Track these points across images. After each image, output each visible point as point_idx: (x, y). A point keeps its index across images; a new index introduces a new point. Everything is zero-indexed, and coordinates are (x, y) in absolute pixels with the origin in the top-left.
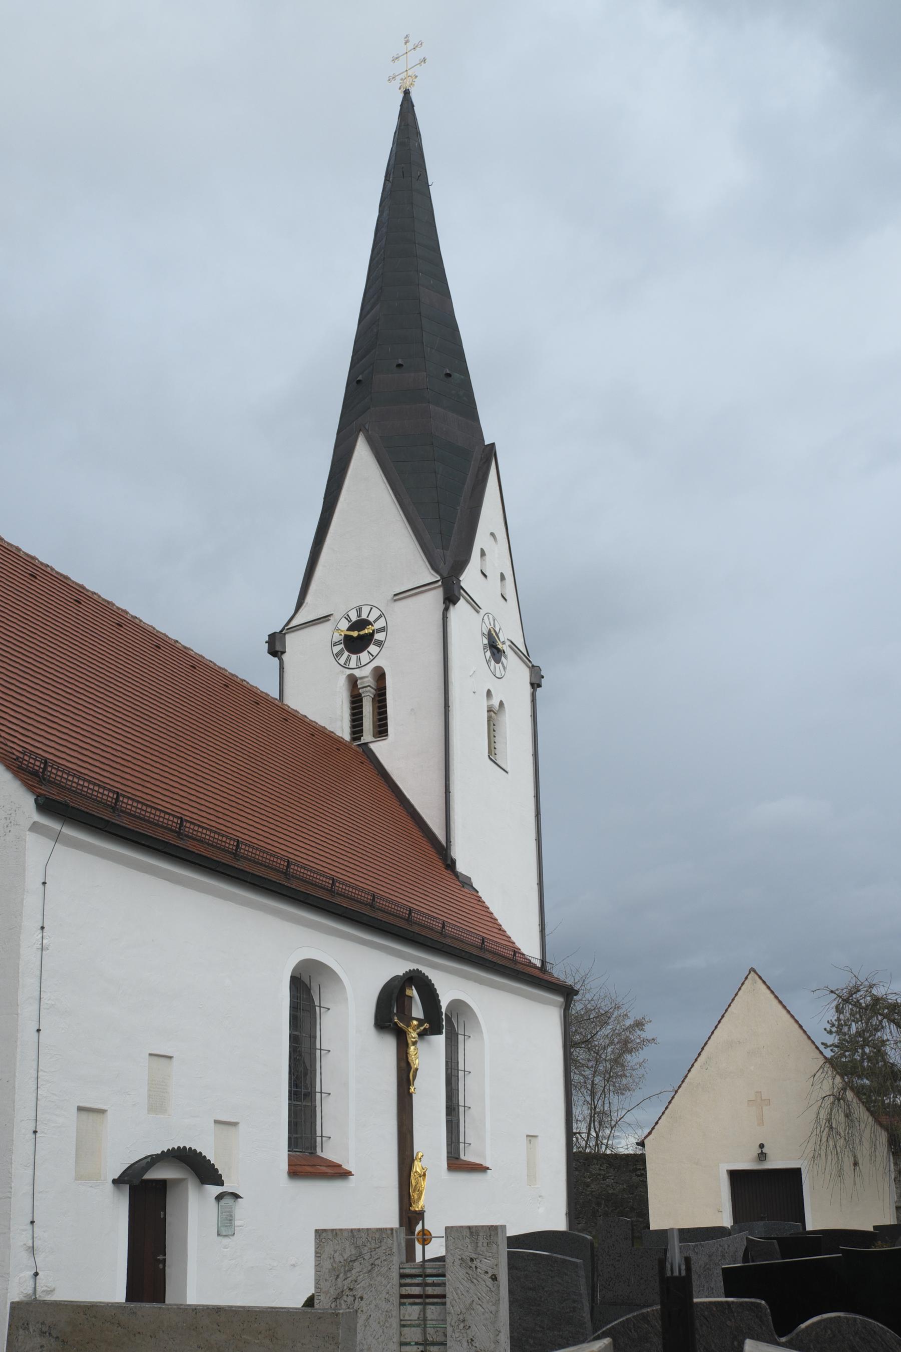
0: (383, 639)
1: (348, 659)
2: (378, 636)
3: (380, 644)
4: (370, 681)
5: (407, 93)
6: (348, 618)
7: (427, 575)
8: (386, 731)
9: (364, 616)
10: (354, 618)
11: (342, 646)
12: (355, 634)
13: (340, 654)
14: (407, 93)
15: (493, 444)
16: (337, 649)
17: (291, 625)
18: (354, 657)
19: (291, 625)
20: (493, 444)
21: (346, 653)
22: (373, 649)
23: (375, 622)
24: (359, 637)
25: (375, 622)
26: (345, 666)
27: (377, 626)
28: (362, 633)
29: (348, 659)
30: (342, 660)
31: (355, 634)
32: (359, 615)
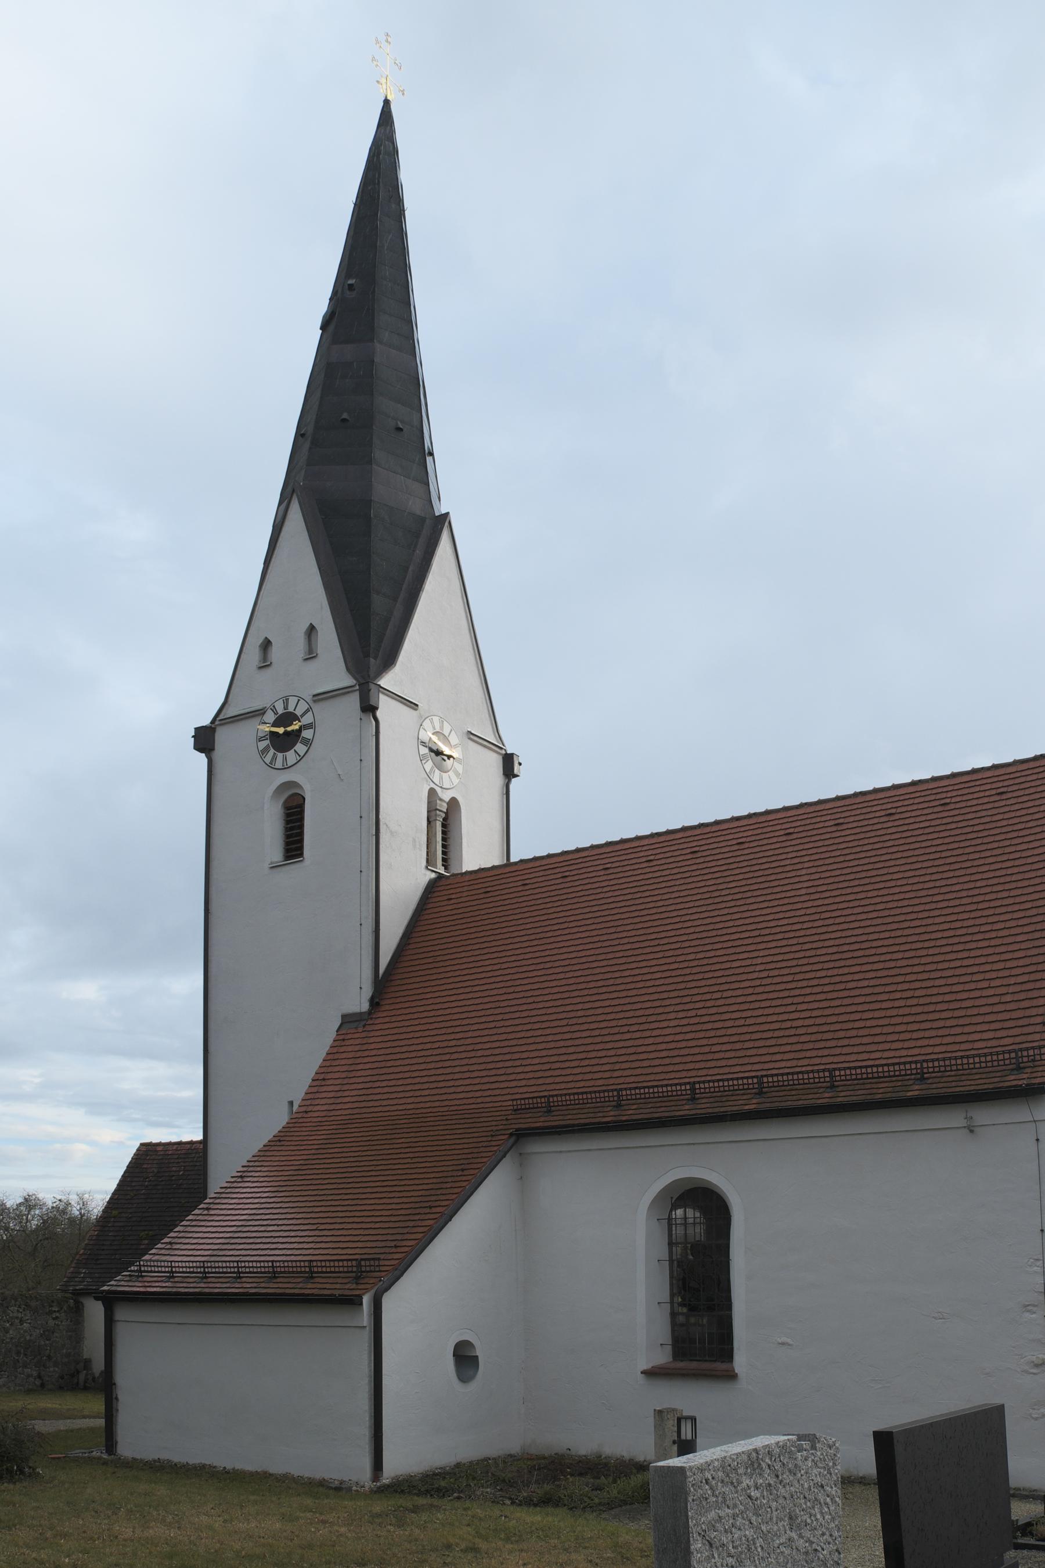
0: (310, 737)
1: (274, 758)
2: (307, 734)
3: (308, 743)
4: (444, 807)
5: (386, 118)
6: (274, 710)
7: (348, 681)
8: (301, 849)
9: (291, 709)
10: (280, 710)
11: (268, 742)
12: (281, 730)
13: (265, 751)
14: (386, 118)
15: (448, 513)
16: (263, 745)
17: (221, 717)
18: (280, 755)
19: (221, 717)
20: (448, 513)
21: (272, 751)
22: (300, 748)
23: (303, 715)
24: (286, 733)
25: (303, 715)
26: (271, 765)
27: (307, 719)
28: (289, 729)
29: (274, 758)
30: (268, 759)
31: (281, 730)
32: (286, 708)
